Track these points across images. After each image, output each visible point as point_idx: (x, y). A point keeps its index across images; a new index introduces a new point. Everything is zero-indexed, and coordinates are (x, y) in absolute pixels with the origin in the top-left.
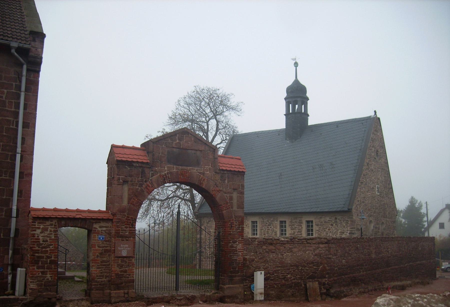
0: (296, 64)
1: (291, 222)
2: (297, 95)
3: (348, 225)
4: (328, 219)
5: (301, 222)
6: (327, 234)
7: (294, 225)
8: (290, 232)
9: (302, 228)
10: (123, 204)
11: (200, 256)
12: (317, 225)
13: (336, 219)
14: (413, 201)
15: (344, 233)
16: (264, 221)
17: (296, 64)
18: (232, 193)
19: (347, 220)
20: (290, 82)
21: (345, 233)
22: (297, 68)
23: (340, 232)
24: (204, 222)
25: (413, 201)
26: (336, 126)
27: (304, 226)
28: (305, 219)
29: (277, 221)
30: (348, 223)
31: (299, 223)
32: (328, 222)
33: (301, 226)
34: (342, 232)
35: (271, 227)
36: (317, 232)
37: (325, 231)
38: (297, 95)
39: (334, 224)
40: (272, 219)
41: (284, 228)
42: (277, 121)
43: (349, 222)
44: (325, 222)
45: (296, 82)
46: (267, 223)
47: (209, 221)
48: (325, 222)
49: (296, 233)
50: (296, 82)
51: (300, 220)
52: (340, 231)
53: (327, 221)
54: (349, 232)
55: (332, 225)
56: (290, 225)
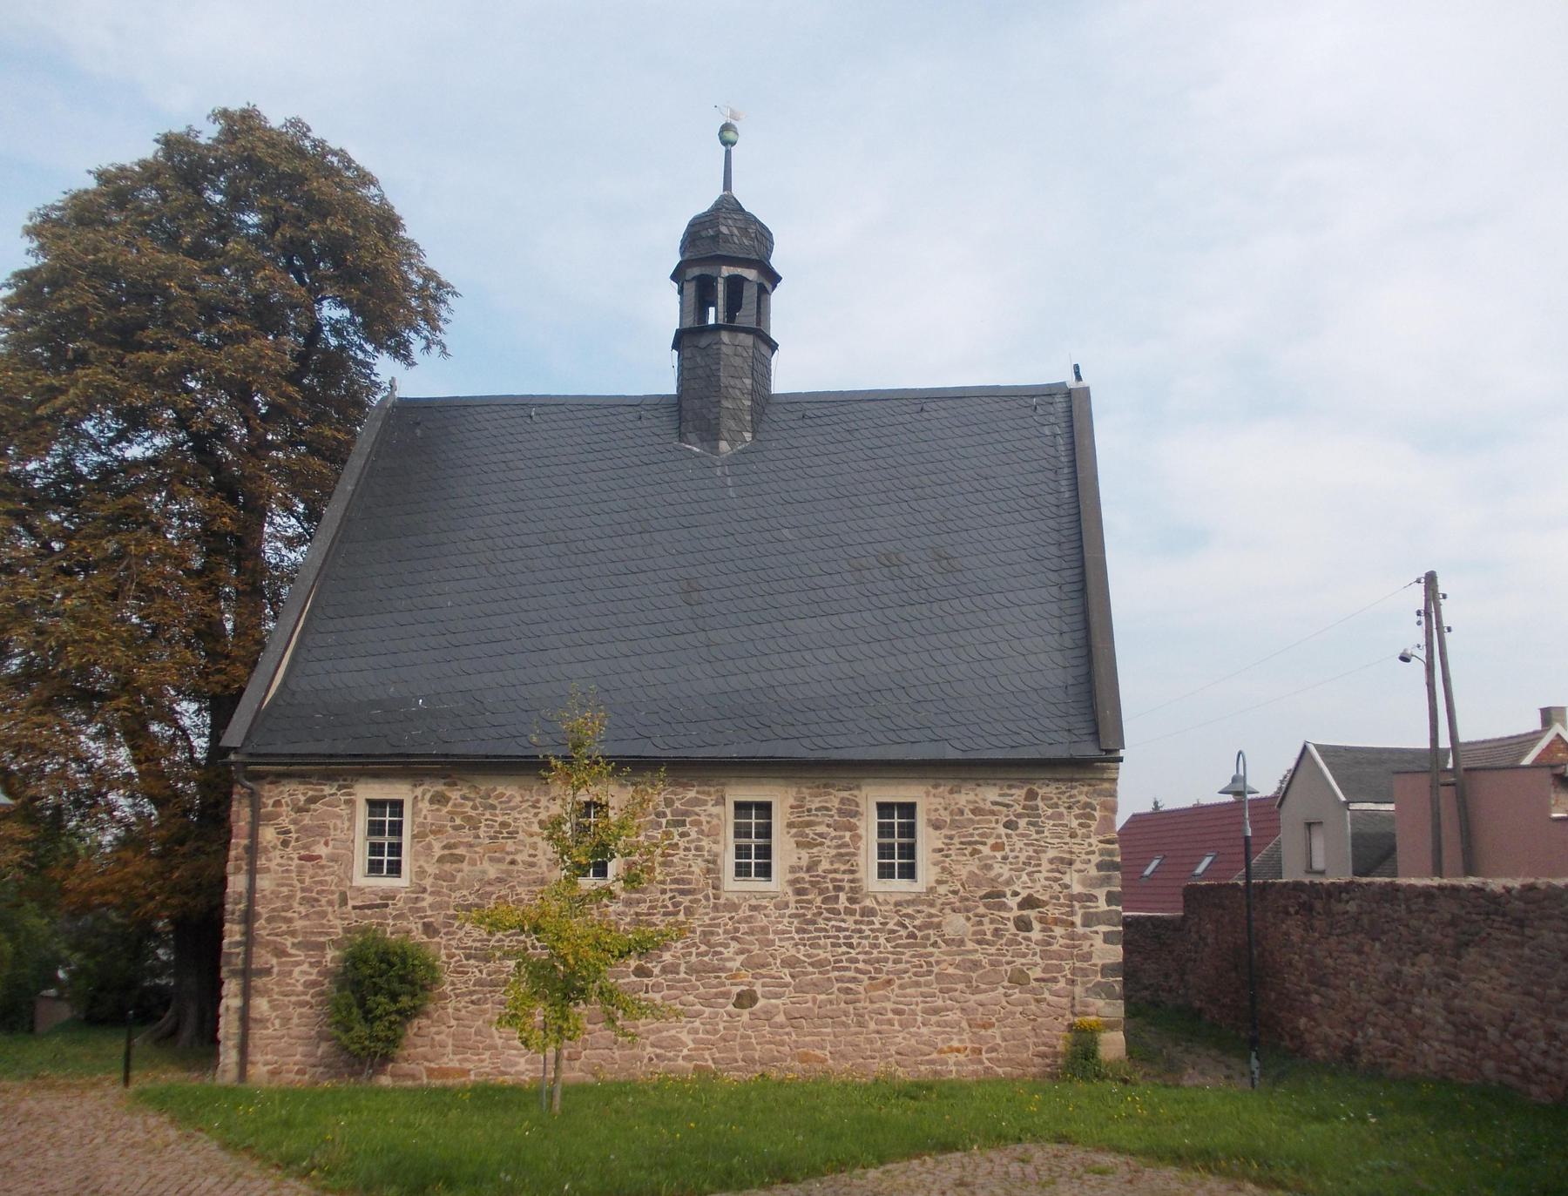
0: (727, 136)
1: (798, 807)
2: (725, 268)
3: (1094, 825)
5: (850, 812)
6: (989, 867)
7: (809, 824)
8: (794, 861)
9: (856, 837)
12: (937, 826)
13: (1031, 795)
14: (31, 232)
15: (1071, 863)
17: (727, 136)
19: (1087, 805)
20: (703, 203)
21: (1078, 865)
22: (734, 149)
23: (1051, 861)
24: (277, 803)
25: (31, 232)
27: (869, 824)
28: (872, 795)
29: (721, 801)
32: (993, 813)
33: (852, 828)
34: (1062, 860)
36: (938, 856)
37: (975, 852)
38: (725, 268)
39: (1022, 823)
40: (692, 794)
42: (640, 358)
43: (1097, 814)
45: (728, 207)
47: (313, 800)
50: (728, 207)
52: (1051, 854)
53: (988, 806)
54: (1095, 859)
56: (790, 825)
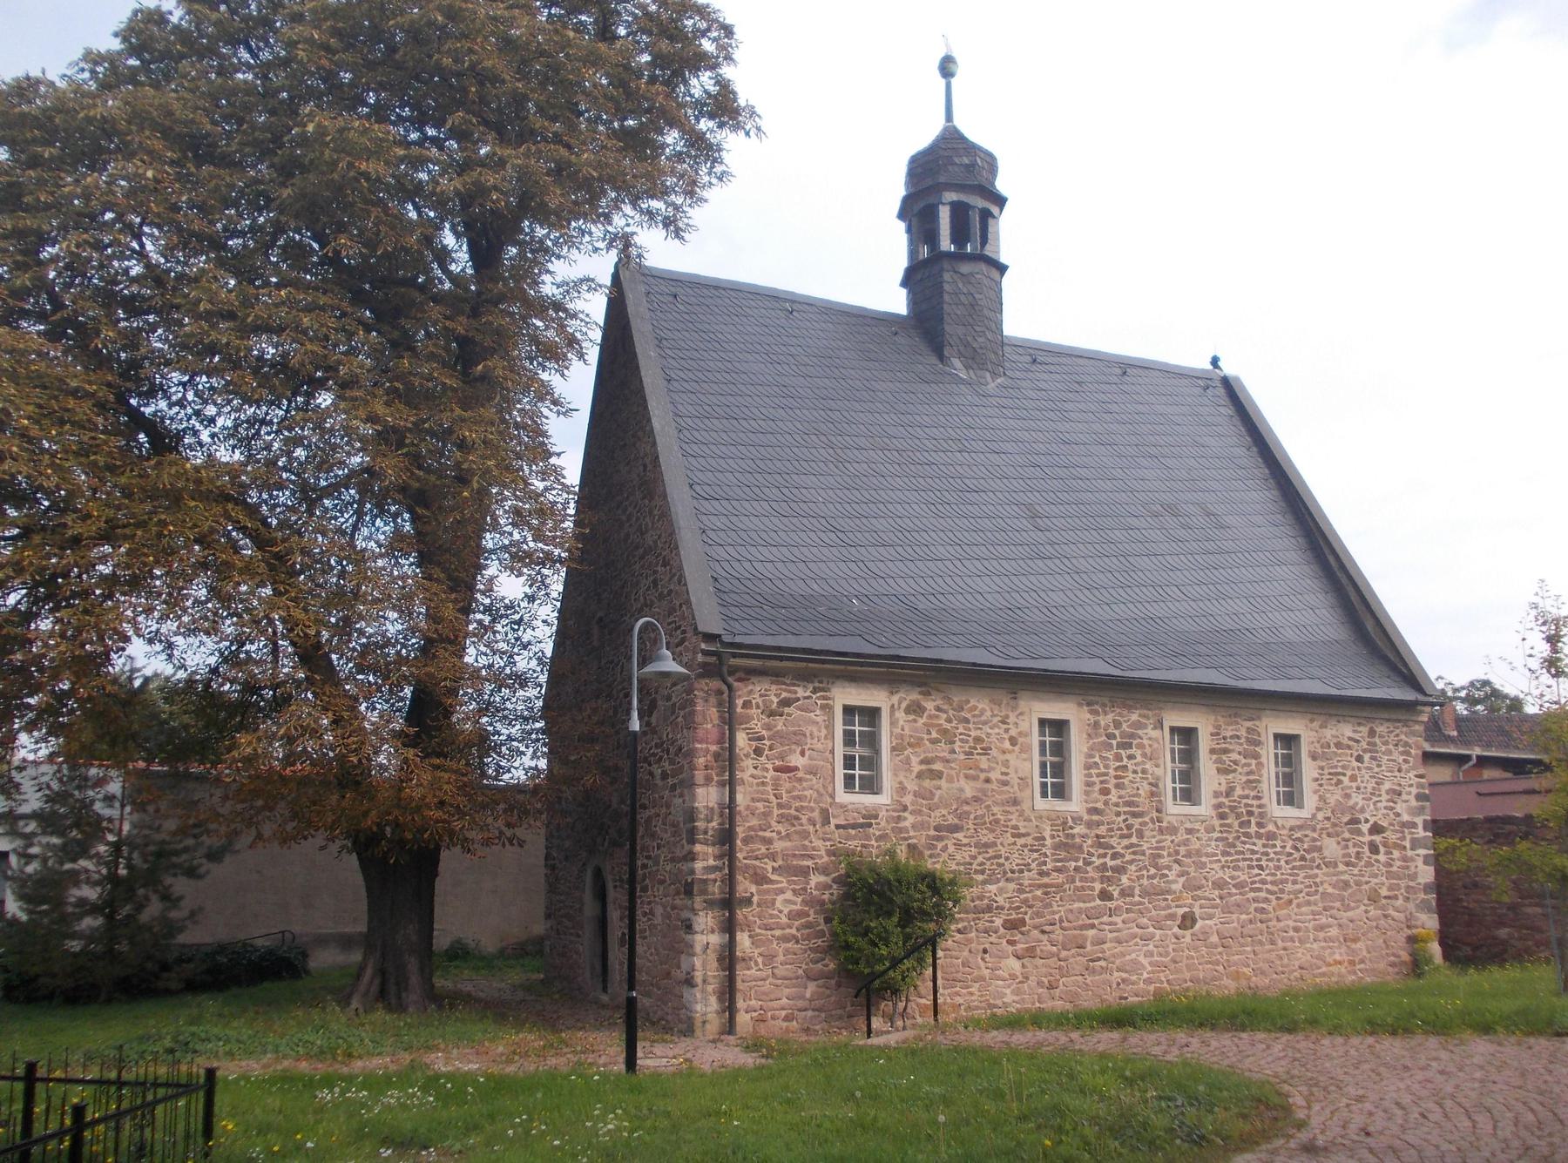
0: (947, 68)
4: (1346, 730)
7: (1226, 751)
8: (1216, 787)
10: (174, 19)
11: (729, 927)
13: (1372, 733)
15: (1400, 794)
16: (1096, 724)
17: (947, 68)
18: (139, 636)
20: (924, 135)
21: (1404, 797)
26: (1119, 371)
28: (1274, 724)
30: (1408, 754)
31: (1249, 741)
33: (1256, 756)
35: (1131, 757)
39: (1367, 757)
40: (1134, 717)
41: (1049, 758)
44: (1338, 745)
46: (1111, 736)
47: (786, 703)
48: (1338, 745)
49: (1239, 791)
51: (1249, 730)
53: (1346, 741)
55: (1359, 759)
